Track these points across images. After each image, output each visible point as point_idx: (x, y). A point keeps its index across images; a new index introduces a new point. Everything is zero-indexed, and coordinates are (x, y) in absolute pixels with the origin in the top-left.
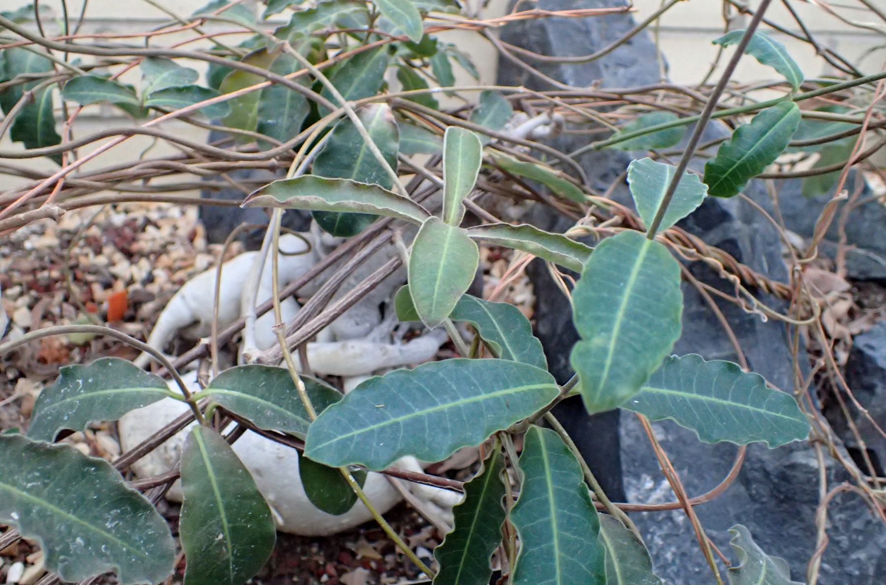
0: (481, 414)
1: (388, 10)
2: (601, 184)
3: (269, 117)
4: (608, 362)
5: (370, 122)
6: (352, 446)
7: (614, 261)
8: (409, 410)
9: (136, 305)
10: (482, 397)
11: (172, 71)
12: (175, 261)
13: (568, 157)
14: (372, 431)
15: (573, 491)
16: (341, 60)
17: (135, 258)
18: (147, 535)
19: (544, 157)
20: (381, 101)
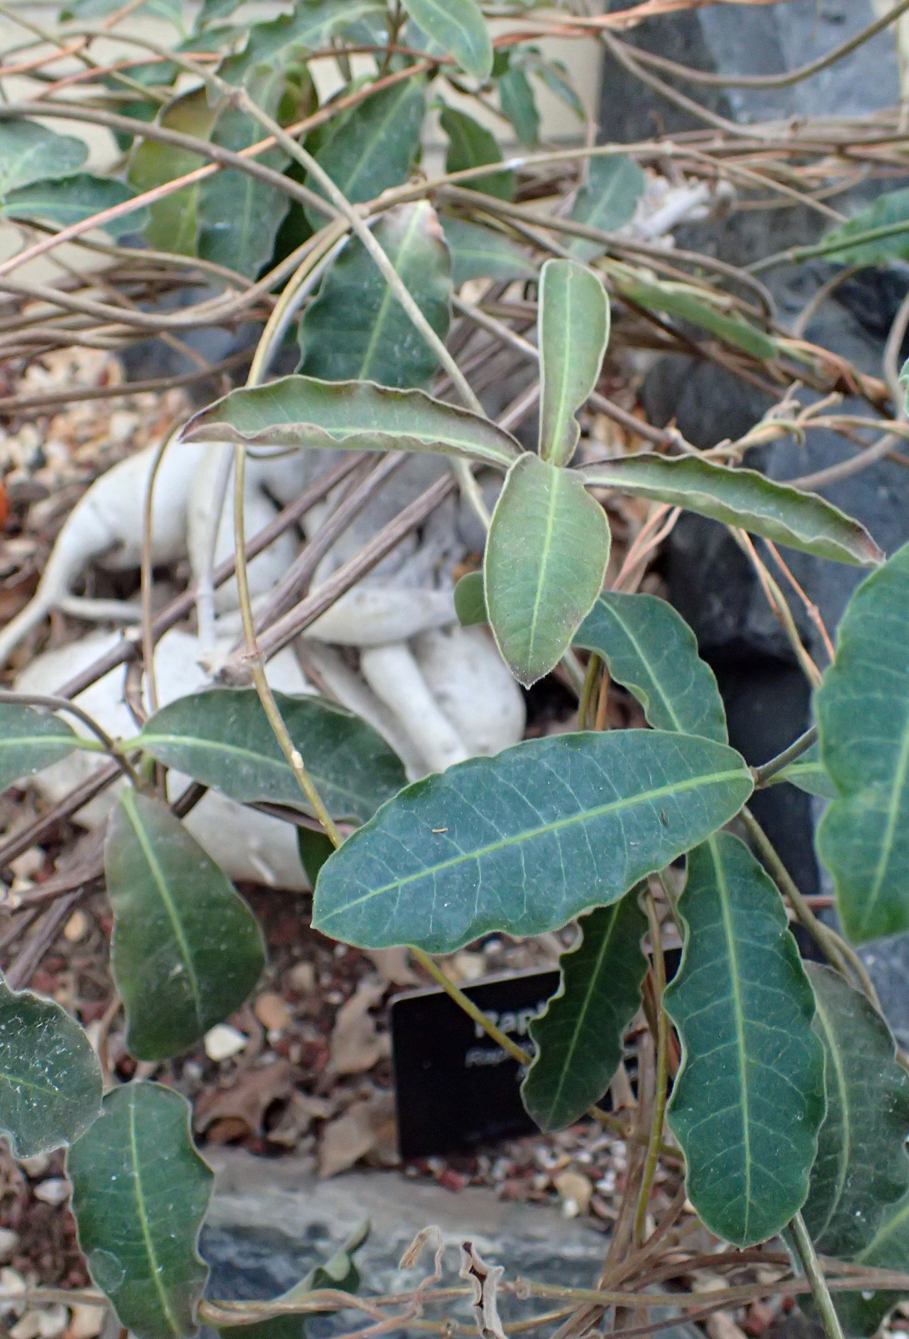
0: (619, 842)
1: (427, 13)
2: (792, 299)
3: (217, 217)
4: (887, 843)
5: (399, 241)
6: (395, 909)
7: (894, 617)
8: (490, 837)
9: (22, 507)
10: (619, 805)
11: (41, 145)
12: (76, 428)
13: (742, 274)
14: (429, 878)
15: (769, 947)
16: (340, 112)
17: (15, 425)
18: (56, 1058)
19: (699, 271)
20: (414, 198)
